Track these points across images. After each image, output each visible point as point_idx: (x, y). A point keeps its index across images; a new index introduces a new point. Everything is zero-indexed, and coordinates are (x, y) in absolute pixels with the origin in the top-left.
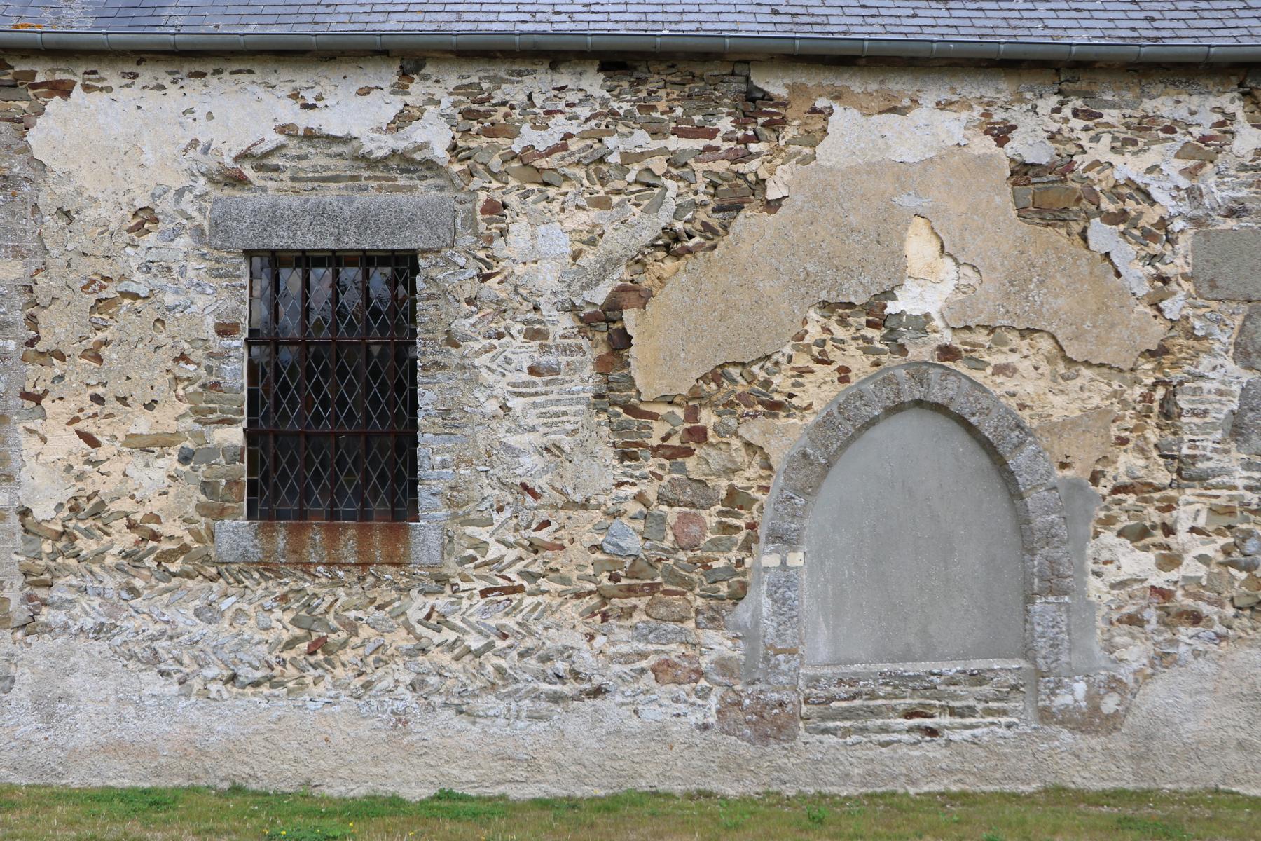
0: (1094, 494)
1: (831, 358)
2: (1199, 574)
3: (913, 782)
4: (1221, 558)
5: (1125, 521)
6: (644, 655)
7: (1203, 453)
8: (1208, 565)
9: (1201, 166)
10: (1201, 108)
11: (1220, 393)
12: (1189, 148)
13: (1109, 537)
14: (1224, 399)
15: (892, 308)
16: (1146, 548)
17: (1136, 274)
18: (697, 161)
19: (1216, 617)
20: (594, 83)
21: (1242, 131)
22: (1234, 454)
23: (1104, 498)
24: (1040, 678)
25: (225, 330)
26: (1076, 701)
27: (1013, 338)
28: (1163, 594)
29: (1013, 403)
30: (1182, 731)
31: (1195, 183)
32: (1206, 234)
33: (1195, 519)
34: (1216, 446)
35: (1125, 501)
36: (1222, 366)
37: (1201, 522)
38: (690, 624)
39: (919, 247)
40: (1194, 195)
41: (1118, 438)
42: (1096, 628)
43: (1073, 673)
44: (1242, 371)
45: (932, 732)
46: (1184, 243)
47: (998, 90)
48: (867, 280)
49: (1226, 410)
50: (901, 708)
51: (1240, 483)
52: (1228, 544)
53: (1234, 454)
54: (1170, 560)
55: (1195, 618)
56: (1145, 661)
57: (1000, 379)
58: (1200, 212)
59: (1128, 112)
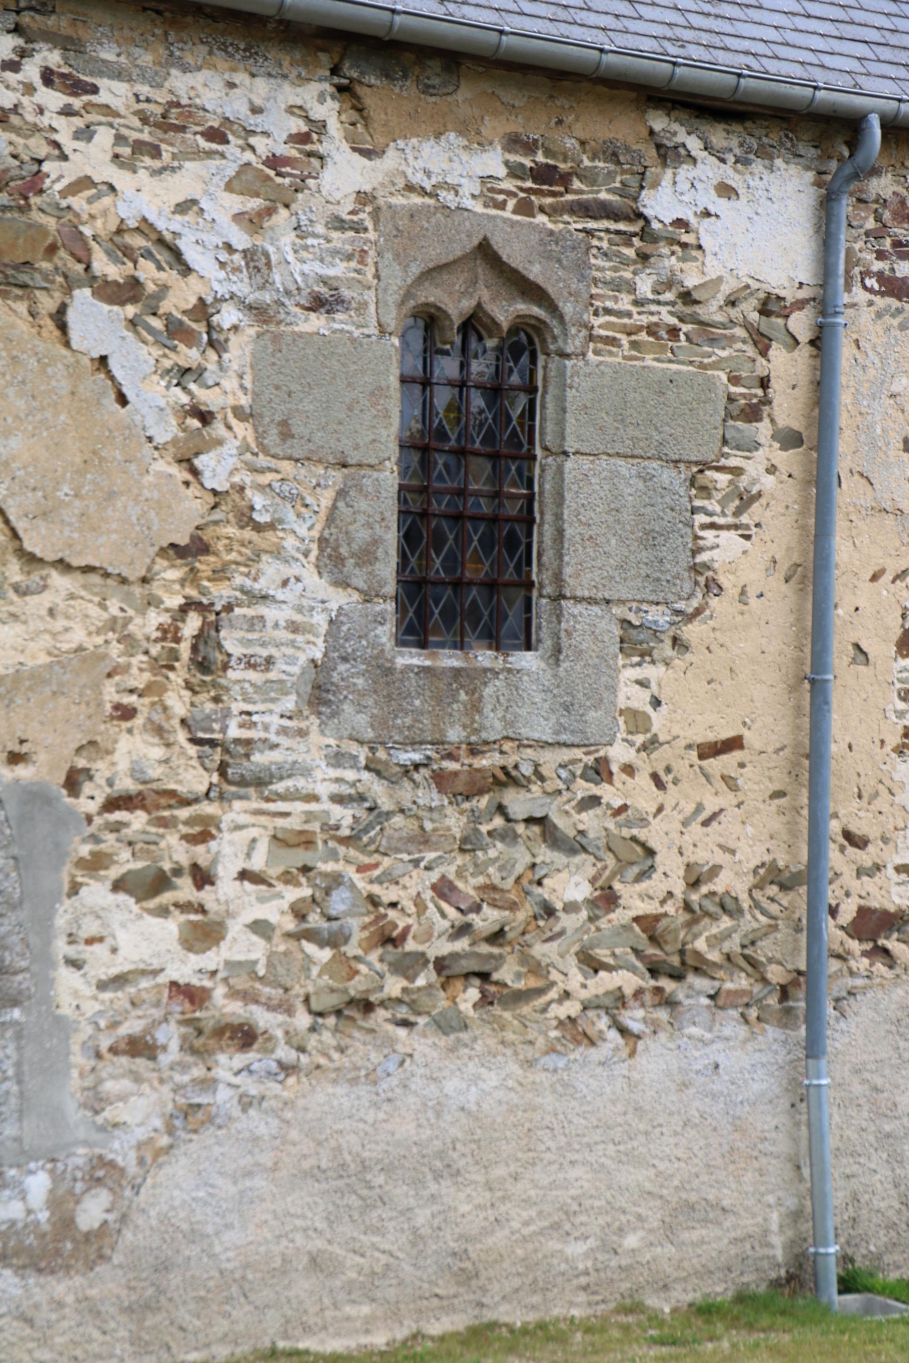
2: (253, 956)
4: (290, 924)
5: (126, 863)
7: (263, 735)
8: (269, 939)
9: (270, 212)
11: (294, 627)
14: (300, 638)
16: (163, 912)
19: (279, 1033)
21: (337, 156)
23: (89, 819)
33: (248, 855)
34: (286, 722)
35: (126, 825)
36: (298, 580)
37: (257, 863)
40: (256, 262)
41: (117, 707)
44: (331, 589)
46: (239, 350)
49: (303, 659)
51: (324, 790)
53: (315, 737)
54: (204, 933)
55: (245, 1036)
58: (267, 297)
59: (144, 90)
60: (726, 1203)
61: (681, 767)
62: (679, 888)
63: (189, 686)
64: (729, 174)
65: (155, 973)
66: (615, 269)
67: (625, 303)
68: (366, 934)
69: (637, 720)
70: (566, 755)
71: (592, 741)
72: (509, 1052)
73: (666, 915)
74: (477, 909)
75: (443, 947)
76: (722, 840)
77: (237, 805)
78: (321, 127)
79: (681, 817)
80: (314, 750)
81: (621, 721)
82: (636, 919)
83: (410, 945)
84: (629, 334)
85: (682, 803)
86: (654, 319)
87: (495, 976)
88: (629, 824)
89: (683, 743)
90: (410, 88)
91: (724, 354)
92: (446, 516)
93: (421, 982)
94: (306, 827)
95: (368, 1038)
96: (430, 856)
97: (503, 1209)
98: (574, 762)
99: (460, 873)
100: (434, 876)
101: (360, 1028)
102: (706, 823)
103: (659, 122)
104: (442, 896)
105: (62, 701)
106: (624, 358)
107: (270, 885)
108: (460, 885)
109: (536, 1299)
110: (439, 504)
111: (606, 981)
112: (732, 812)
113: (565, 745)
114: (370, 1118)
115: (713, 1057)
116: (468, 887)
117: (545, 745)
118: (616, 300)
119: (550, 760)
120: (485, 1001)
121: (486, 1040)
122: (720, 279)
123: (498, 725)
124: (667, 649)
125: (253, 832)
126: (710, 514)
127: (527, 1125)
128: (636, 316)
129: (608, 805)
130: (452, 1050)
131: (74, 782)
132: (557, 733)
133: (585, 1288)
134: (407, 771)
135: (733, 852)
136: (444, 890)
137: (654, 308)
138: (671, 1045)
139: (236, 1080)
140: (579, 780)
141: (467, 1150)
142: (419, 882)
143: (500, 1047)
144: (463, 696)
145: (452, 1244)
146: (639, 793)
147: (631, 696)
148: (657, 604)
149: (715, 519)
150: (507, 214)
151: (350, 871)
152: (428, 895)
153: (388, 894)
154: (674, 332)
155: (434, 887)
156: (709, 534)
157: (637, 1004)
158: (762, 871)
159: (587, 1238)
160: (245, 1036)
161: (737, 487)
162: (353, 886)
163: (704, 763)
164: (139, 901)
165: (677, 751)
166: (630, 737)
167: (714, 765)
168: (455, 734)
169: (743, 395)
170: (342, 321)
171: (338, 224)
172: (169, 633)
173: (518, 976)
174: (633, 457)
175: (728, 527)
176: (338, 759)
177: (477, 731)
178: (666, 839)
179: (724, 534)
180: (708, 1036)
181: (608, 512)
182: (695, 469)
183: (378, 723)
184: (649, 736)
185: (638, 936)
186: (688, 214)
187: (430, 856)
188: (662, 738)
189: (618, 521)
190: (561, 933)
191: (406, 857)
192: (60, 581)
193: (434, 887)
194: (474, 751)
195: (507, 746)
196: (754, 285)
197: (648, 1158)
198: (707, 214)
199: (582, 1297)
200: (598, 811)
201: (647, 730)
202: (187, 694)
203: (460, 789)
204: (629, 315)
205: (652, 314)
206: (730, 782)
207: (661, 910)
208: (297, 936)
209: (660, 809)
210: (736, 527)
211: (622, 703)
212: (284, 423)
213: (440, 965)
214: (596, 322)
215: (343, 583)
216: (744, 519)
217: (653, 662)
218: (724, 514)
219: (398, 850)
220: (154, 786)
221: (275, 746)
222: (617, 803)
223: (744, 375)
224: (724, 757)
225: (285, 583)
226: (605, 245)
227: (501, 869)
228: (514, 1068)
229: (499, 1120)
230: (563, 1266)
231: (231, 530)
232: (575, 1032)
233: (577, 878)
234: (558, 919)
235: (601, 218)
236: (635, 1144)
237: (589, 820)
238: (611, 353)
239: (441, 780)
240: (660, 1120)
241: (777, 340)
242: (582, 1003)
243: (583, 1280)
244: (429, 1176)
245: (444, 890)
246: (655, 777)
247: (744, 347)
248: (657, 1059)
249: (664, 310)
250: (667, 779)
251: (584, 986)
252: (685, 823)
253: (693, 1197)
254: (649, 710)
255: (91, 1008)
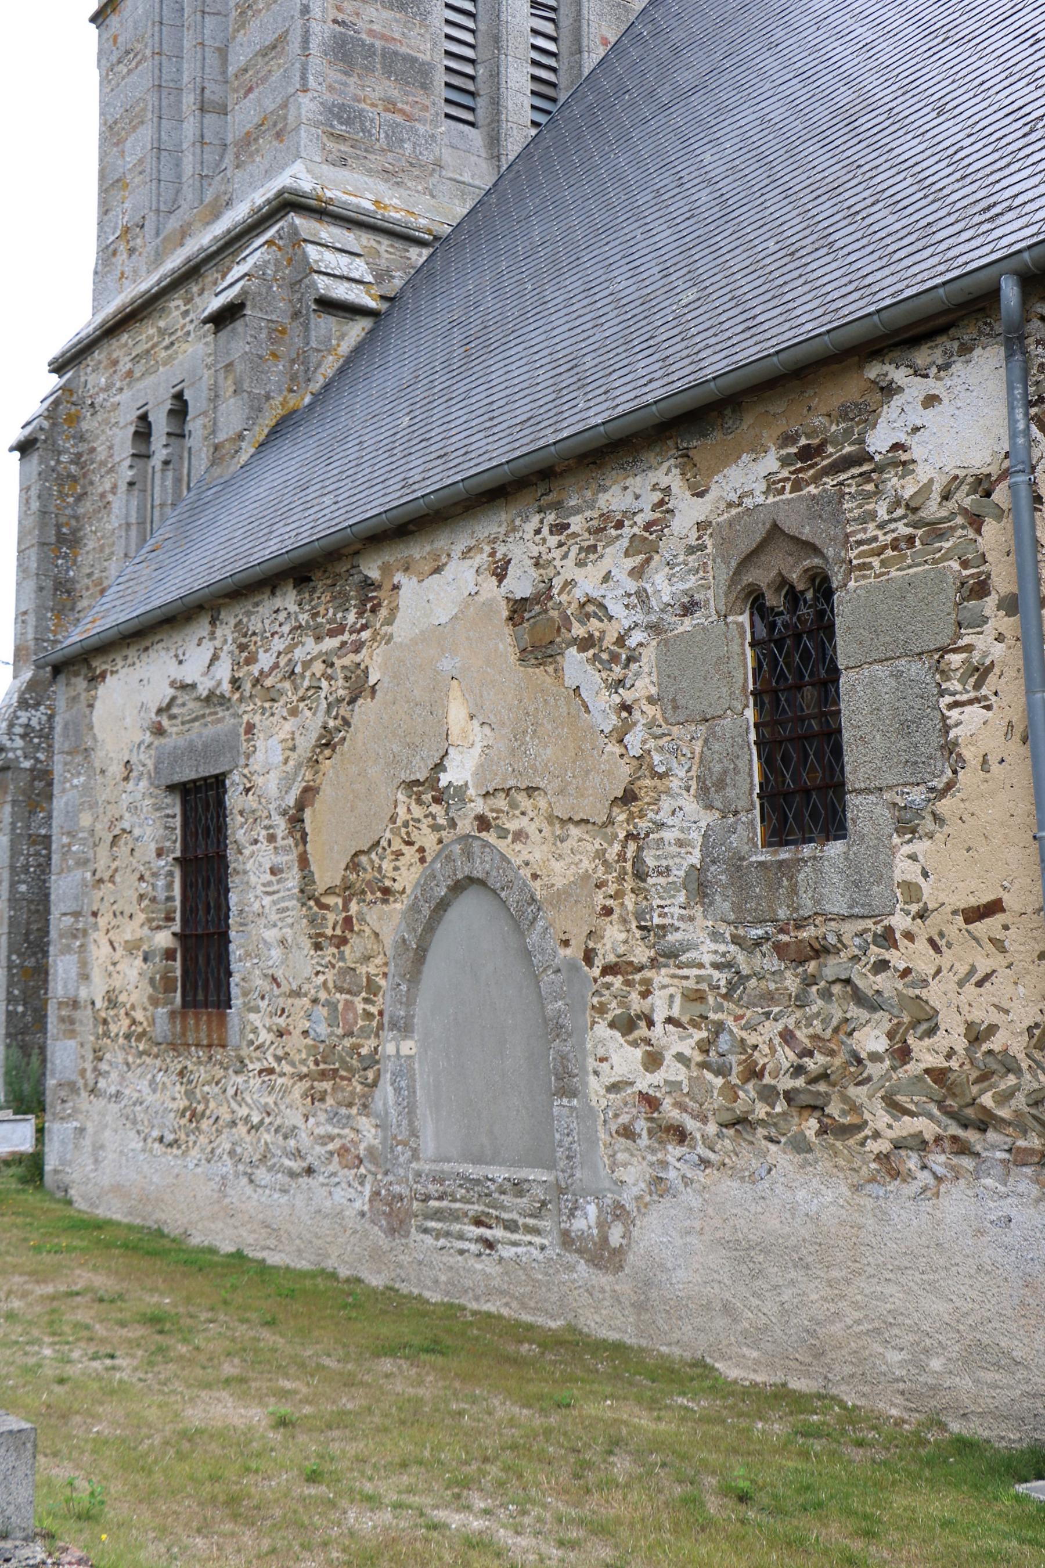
0: (586, 976)
1: (413, 839)
2: (679, 1078)
3: (477, 1299)
4: (698, 1057)
5: (615, 1010)
6: (332, 1138)
7: (670, 921)
8: (688, 1067)
9: (648, 561)
10: (631, 493)
11: (680, 843)
12: (637, 539)
13: (602, 1030)
14: (683, 851)
15: (444, 779)
16: (634, 1044)
17: (603, 704)
18: (339, 657)
19: (698, 1136)
20: (288, 600)
21: (681, 506)
22: (700, 921)
23: (595, 980)
24: (561, 1197)
25: (160, 853)
26: (590, 1228)
27: (521, 798)
28: (651, 1102)
29: (525, 873)
30: (674, 1281)
31: (641, 583)
32: (666, 642)
33: (670, 1007)
34: (683, 912)
35: (612, 985)
36: (681, 809)
37: (675, 1012)
38: (354, 1111)
39: (457, 713)
40: (642, 596)
41: (604, 907)
42: (598, 1139)
43: (585, 1193)
44: (702, 812)
45: (490, 1245)
46: (649, 656)
47: (490, 526)
48: (424, 754)
49: (685, 866)
50: (471, 1214)
51: (707, 959)
52: (702, 1040)
53: (700, 921)
54: (653, 1061)
55: (681, 1135)
56: (643, 1185)
57: (518, 846)
58: (654, 618)
59: (588, 514)
60: (1017, 1354)
61: (951, 931)
62: (961, 1044)
63: (633, 891)
64: (931, 386)
65: (632, 1084)
66: (860, 506)
67: (872, 530)
68: (741, 1068)
69: (912, 892)
70: (861, 925)
71: (877, 912)
72: (841, 1175)
73: (950, 1069)
74: (810, 1054)
75: (787, 1083)
76: (996, 1000)
77: (663, 971)
78: (667, 491)
79: (956, 978)
80: (698, 930)
81: (898, 892)
82: (927, 1071)
83: (767, 1080)
84: (879, 555)
85: (957, 965)
86: (894, 535)
87: (827, 1111)
88: (913, 985)
89: (948, 909)
90: (718, 435)
91: (947, 545)
92: (791, 740)
93: (778, 1109)
94: (699, 987)
95: (750, 1148)
96: (776, 1010)
97: (840, 1305)
98: (866, 930)
99: (798, 1023)
100: (779, 1026)
101: (745, 1140)
102: (979, 984)
103: (873, 371)
104: (787, 1042)
105: (580, 906)
106: (877, 576)
107: (685, 1028)
108: (798, 1033)
109: (866, 1389)
110: (785, 731)
111: (909, 1125)
112: (1002, 972)
113: (857, 917)
114: (753, 1209)
115: (1007, 1211)
116: (801, 1035)
117: (844, 918)
118: (865, 530)
119: (849, 929)
120: (822, 1131)
121: (825, 1165)
122: (931, 481)
123: (809, 903)
124: (928, 824)
125: (671, 990)
126: (953, 694)
127: (854, 1239)
128: (881, 538)
129: (896, 969)
130: (802, 1167)
131: (589, 957)
132: (851, 907)
133: (903, 1393)
134: (758, 943)
135: (1007, 1012)
136: (787, 1037)
137: (892, 526)
138: (970, 1193)
139: (678, 1165)
140: (872, 946)
141: (812, 1250)
142: (771, 1029)
143: (835, 1170)
144: (785, 883)
145: (806, 1323)
146: (916, 955)
147: (904, 870)
148: (918, 784)
149: (958, 697)
150: (787, 496)
151: (730, 1022)
152: (777, 1040)
153: (752, 1039)
154: (910, 540)
155: (781, 1034)
156: (954, 714)
157: (939, 1149)
158: (1037, 1032)
159: (902, 1349)
160: (681, 1135)
161: (970, 663)
162: (731, 1031)
163: (970, 927)
164: (623, 1035)
165: (945, 917)
166: (906, 907)
167: (980, 928)
168: (782, 913)
169: (972, 576)
170: (698, 618)
171: (691, 550)
172: (621, 857)
173: (844, 1113)
174: (886, 660)
175: (970, 702)
176: (716, 936)
177: (796, 910)
178: (945, 999)
179: (968, 709)
180: (1002, 1189)
181: (871, 713)
182: (936, 657)
183: (737, 908)
184: (921, 904)
185: (930, 1087)
186: (902, 437)
187: (776, 1010)
188: (930, 906)
189: (879, 719)
190: (869, 1079)
191: (760, 1010)
192: (574, 831)
193: (781, 1034)
194: (798, 927)
195: (819, 920)
196: (961, 473)
197: (947, 1292)
198: (916, 429)
199: (899, 1400)
200: (889, 973)
201: (919, 901)
202: (633, 895)
203: (793, 957)
204: (875, 539)
205: (893, 531)
206: (999, 945)
207: (947, 1064)
208: (704, 1065)
209: (938, 971)
210: (977, 700)
211: (898, 877)
212: (674, 700)
213: (789, 1096)
214: (852, 554)
215: (709, 807)
216: (984, 691)
217: (920, 838)
218: (968, 692)
219: (755, 1005)
220: (624, 959)
221: (678, 929)
222: (902, 966)
223: (970, 556)
224: (987, 920)
225: (673, 813)
226: (853, 490)
227: (823, 1021)
228: (844, 1190)
229: (833, 1230)
230: (884, 1368)
231: (647, 782)
232: (889, 1166)
233: (877, 1032)
234: (865, 1066)
235: (848, 468)
236: (937, 1276)
237: (881, 981)
238: (864, 577)
239: (780, 949)
240: (958, 1259)
241: (988, 515)
242: (891, 1141)
243: (901, 1386)
244: (790, 1265)
245: (787, 1037)
246: (931, 941)
247: (965, 532)
248: (957, 1204)
249: (900, 525)
250: (942, 943)
251: (890, 1127)
252: (961, 984)
253: (985, 1340)
254: (921, 880)
255: (604, 1103)
